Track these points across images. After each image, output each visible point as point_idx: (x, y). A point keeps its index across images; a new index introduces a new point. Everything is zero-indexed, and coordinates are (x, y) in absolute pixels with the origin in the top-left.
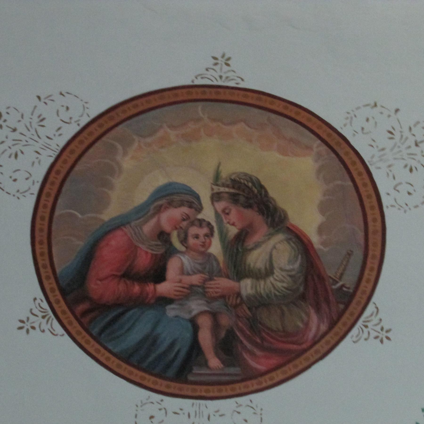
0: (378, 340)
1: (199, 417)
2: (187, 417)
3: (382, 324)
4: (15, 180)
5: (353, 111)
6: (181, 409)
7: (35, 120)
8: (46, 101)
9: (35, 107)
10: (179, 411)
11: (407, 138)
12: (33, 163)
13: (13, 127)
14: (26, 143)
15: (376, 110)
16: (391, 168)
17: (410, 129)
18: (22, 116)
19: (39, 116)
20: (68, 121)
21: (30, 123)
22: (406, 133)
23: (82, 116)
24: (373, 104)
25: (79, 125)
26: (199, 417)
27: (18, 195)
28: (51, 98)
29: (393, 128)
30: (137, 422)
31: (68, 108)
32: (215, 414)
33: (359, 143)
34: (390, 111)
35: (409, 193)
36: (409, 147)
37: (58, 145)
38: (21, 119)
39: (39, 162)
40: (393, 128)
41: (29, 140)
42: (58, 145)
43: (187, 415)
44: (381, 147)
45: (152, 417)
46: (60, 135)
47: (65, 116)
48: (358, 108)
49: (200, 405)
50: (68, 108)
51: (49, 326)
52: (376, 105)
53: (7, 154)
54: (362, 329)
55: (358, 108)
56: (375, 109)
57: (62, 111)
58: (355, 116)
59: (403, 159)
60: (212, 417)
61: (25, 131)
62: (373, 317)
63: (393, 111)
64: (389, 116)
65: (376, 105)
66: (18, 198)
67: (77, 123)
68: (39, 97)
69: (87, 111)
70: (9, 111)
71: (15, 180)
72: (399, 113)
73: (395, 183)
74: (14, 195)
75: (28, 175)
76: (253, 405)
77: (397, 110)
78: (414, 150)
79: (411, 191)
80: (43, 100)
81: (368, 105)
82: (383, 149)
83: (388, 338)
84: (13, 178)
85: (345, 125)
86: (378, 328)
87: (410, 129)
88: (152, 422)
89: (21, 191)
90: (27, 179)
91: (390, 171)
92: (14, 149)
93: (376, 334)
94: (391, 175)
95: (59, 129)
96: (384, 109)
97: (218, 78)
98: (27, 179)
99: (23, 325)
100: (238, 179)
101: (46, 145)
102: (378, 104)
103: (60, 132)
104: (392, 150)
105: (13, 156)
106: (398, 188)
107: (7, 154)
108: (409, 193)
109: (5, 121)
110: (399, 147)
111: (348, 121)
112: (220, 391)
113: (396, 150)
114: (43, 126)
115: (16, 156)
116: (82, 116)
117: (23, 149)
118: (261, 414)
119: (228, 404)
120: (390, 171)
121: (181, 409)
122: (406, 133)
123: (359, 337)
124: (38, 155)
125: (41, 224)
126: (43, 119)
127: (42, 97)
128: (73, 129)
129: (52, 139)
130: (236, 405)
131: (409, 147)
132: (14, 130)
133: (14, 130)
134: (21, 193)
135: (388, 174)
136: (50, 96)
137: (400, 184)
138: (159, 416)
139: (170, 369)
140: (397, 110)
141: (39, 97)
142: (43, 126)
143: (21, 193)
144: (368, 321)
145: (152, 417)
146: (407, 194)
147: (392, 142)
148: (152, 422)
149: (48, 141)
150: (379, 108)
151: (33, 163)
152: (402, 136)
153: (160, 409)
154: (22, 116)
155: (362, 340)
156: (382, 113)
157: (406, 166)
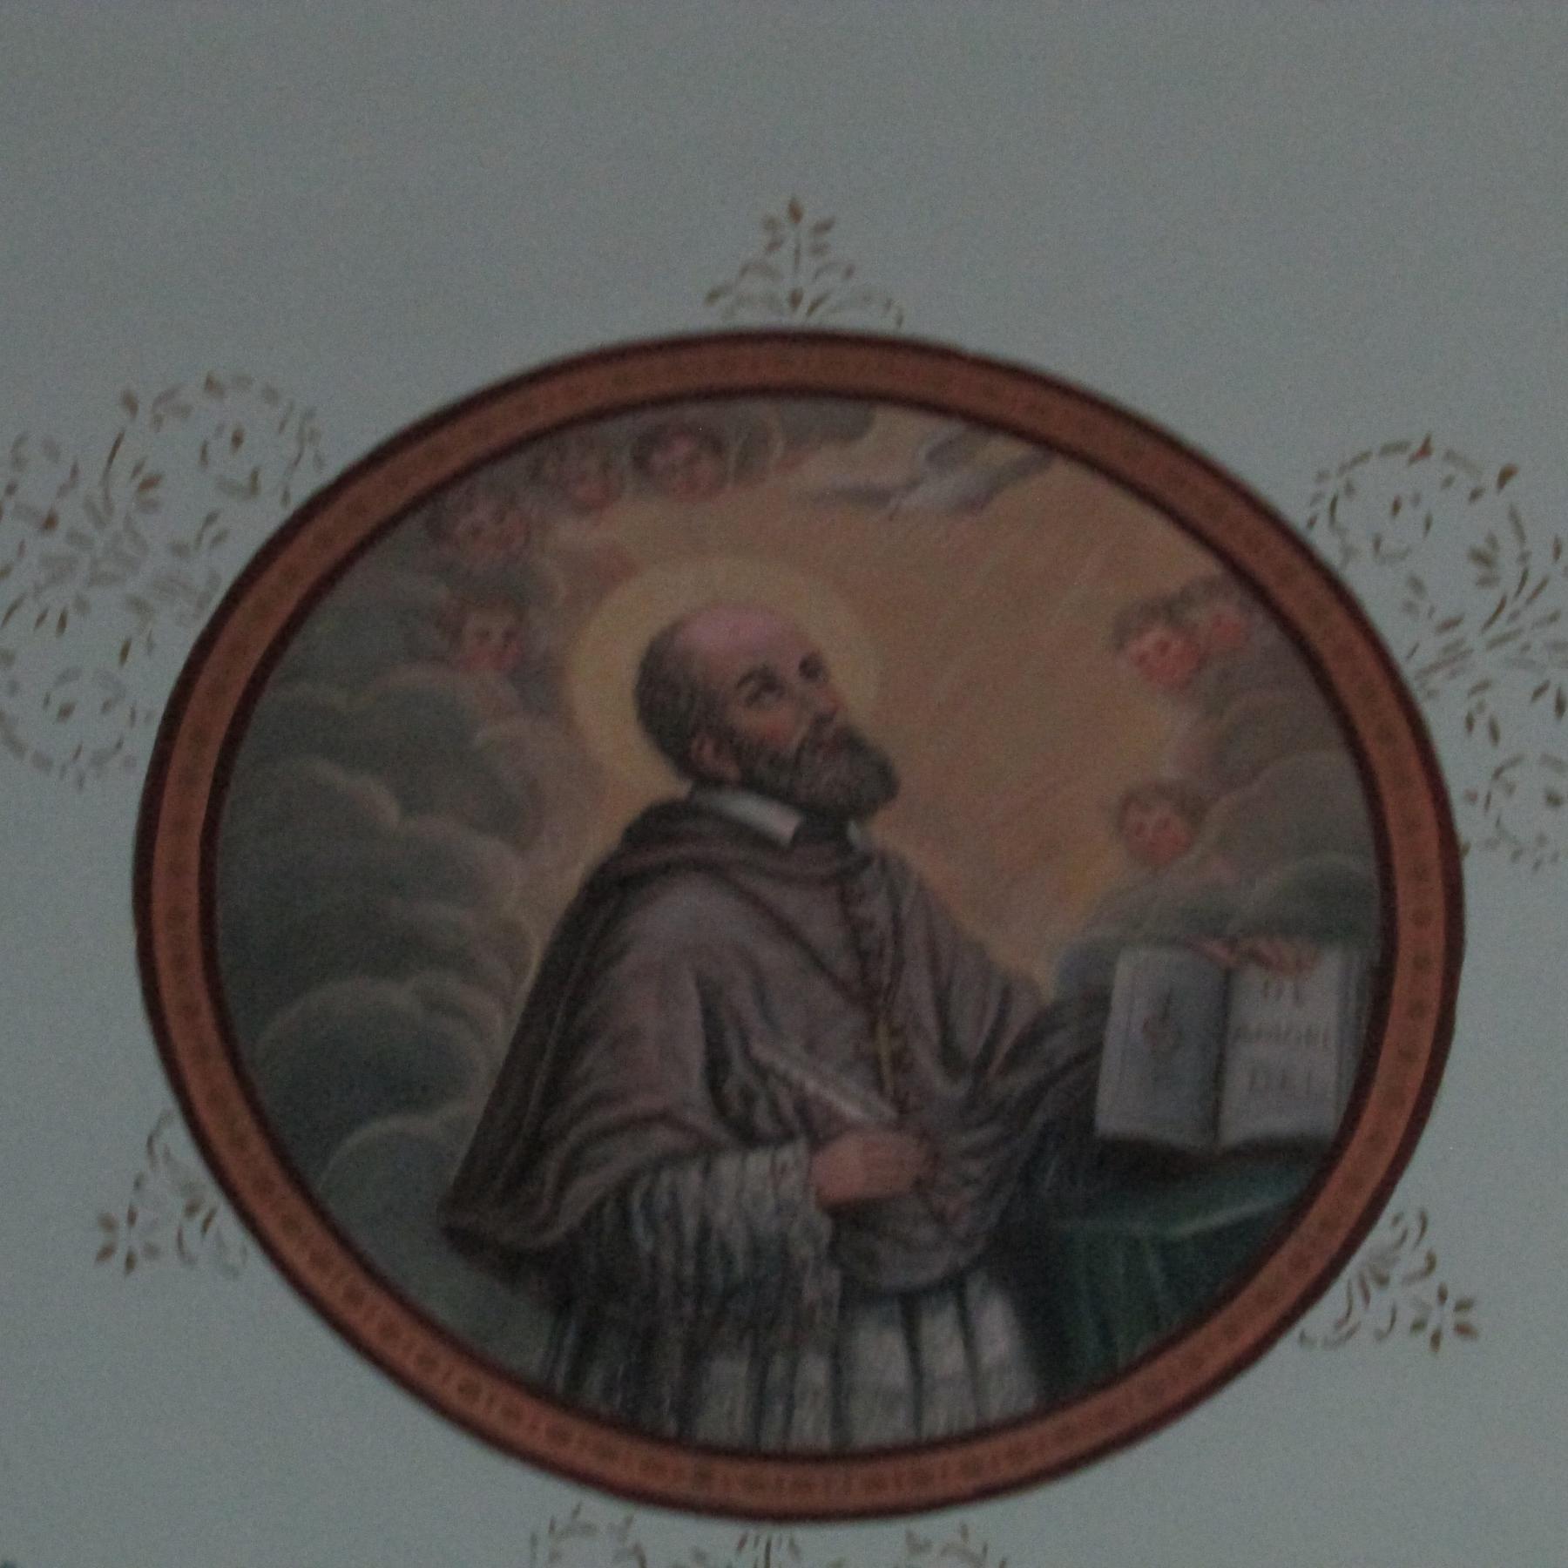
7: (124, 490)
15: (1433, 468)
19: (137, 469)
24: (1416, 447)
37: (742, 1544)
42: (742, 1544)
46: (1470, 723)
53: (29, 613)
54: (1363, 1285)
63: (1491, 479)
64: (1475, 495)
65: (1425, 451)
72: (1513, 485)
73: (1500, 756)
77: (1506, 476)
78: (71, 514)
81: (1399, 447)
82: (1450, 624)
83: (1436, 1339)
90: (1377, 544)
95: (211, 519)
99: (117, 1245)
102: (1435, 444)
106: (1510, 775)
112: (318, 1261)
123: (1345, 1329)
124: (1439, 617)
128: (266, 518)
137: (1515, 762)
139: (1395, 925)
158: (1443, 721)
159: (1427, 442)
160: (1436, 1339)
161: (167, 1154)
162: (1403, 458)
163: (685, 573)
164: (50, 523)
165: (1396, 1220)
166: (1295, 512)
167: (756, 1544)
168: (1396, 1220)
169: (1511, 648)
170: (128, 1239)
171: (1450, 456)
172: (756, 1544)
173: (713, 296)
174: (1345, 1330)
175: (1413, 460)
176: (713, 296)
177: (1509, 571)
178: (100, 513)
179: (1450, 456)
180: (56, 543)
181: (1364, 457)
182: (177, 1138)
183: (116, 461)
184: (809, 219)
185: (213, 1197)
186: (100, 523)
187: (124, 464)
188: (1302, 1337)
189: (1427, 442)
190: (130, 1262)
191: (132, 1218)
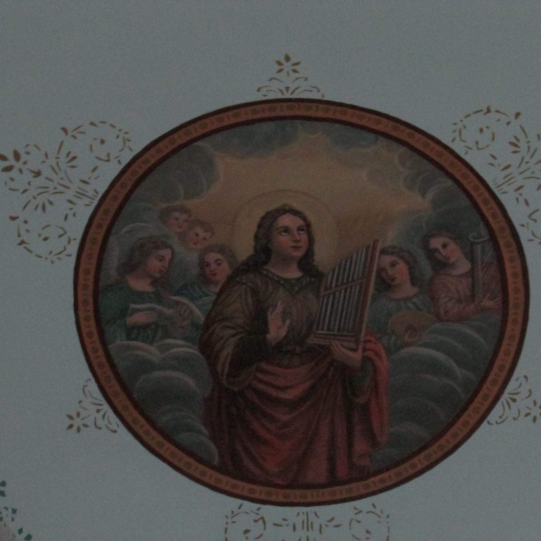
2: (292, 529)
3: (533, 397)
4: (46, 239)
5: (461, 121)
6: (285, 520)
7: (63, 159)
8: (75, 133)
9: (62, 143)
13: (36, 171)
14: (55, 191)
15: (493, 115)
18: (46, 155)
21: (58, 163)
24: (485, 110)
25: (119, 162)
26: (308, 530)
28: (79, 130)
29: (37, 207)
30: (229, 539)
31: (102, 142)
32: (328, 523)
33: (478, 161)
38: (45, 159)
39: (74, 215)
41: (58, 186)
43: (291, 527)
45: (247, 531)
49: (307, 513)
51: (106, 422)
52: (489, 111)
53: (521, 136)
54: (508, 403)
58: (465, 127)
61: (53, 176)
64: (508, 124)
67: (118, 159)
68: (65, 130)
69: (128, 144)
70: (28, 149)
71: (46, 239)
75: (62, 232)
76: (378, 511)
77: (518, 115)
78: (46, 172)
80: (70, 133)
84: (43, 236)
85: (454, 140)
88: (247, 538)
90: (60, 236)
92: (41, 199)
95: (95, 169)
96: (500, 114)
97: (284, 91)
98: (60, 236)
105: (40, 208)
107: (521, 136)
109: (25, 163)
111: (457, 134)
113: (524, 167)
115: (44, 208)
117: (52, 198)
120: (521, 195)
121: (285, 520)
125: (492, 208)
126: (74, 158)
127: (70, 129)
132: (38, 174)
133: (38, 174)
135: (517, 199)
138: (256, 529)
140: (518, 115)
141: (65, 130)
144: (517, 394)
145: (247, 531)
147: (518, 156)
148: (247, 538)
149: (83, 185)
150: (493, 114)
152: (529, 148)
153: (256, 521)
154: (46, 155)
158: (508, 201)
161: (311, 91)
162: (482, 113)
163: (244, 186)
165: (265, 96)
168: (265, 96)
169: (528, 174)
170: (77, 422)
174: (502, 420)
175: (486, 114)
180: (40, 181)
182: (493, 416)
183: (61, 151)
187: (64, 152)
188: (488, 422)
190: (79, 430)
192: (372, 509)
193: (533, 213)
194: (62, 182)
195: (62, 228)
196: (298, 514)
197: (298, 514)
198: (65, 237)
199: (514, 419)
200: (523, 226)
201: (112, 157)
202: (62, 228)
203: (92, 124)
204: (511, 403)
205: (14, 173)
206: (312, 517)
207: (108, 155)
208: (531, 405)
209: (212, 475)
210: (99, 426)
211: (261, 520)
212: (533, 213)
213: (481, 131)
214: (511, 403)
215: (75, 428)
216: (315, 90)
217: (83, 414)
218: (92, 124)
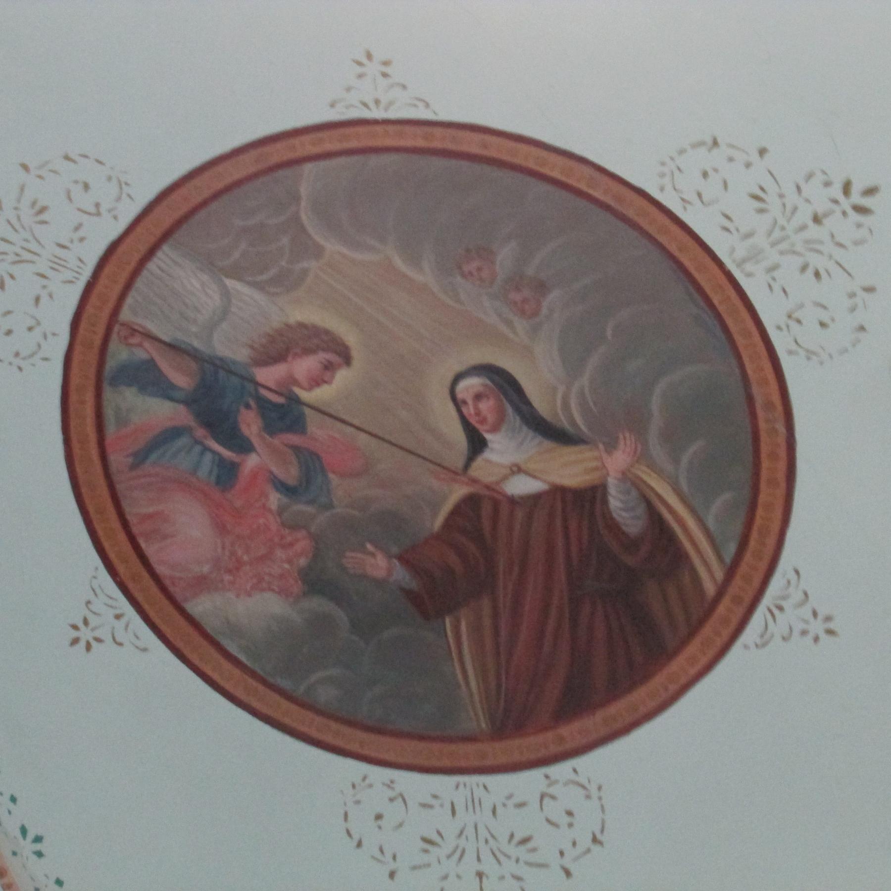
0: (809, 639)
1: (51, 261)
5: (672, 159)
7: (816, 261)
10: (430, 801)
11: (795, 209)
12: (37, 299)
14: (17, 258)
15: (585, 841)
16: (776, 274)
17: (799, 188)
19: (34, 204)
20: (92, 210)
22: (792, 198)
23: (119, 199)
24: (709, 141)
26: (51, 261)
27: (17, 361)
29: (762, 189)
34: (747, 153)
35: (823, 325)
36: (803, 228)
40: (762, 189)
44: (743, 230)
46: (435, 797)
47: (86, 201)
48: (682, 152)
50: (86, 187)
52: (715, 143)
53: (769, 184)
55: (682, 152)
56: (715, 151)
57: (77, 190)
59: (794, 252)
60: (499, 811)
62: (791, 590)
63: (567, 862)
64: (748, 165)
66: (20, 369)
68: (25, 167)
72: (767, 156)
74: (10, 364)
75: (32, 322)
77: (762, 152)
78: (814, 231)
79: (826, 320)
81: (701, 144)
83: (75, 627)
86: (806, 612)
87: (799, 188)
89: (23, 354)
91: (774, 279)
93: (801, 626)
94: (776, 287)
97: (372, 105)
100: (356, 513)
101: (56, 260)
103: (81, 233)
104: (770, 233)
107: (769, 184)
108: (823, 325)
110: (783, 228)
114: (44, 222)
116: (119, 199)
118: (600, 798)
119: (528, 782)
122: (792, 198)
124: (44, 282)
127: (32, 166)
129: (452, 804)
130: (546, 782)
131: (803, 228)
134: (24, 359)
136: (47, 163)
142: (44, 222)
143: (24, 359)
146: (818, 326)
149: (460, 809)
151: (37, 299)
155: (777, 639)
156: (731, 159)
157: (804, 268)
159: (601, 843)
160: (75, 627)
161: (415, 106)
164: (817, 220)
166: (582, 762)
167: (78, 267)
169: (784, 246)
171: (588, 851)
172: (78, 267)
173: (332, 105)
176: (332, 105)
177: (512, 850)
178: (812, 245)
179: (588, 851)
181: (603, 809)
184: (74, 634)
185: (767, 600)
186: (807, 242)
189: (601, 843)
190: (88, 647)
191: (385, 75)
192: (573, 776)
193: (89, 214)
194: (25, 245)
195: (33, 317)
196: (457, 787)
197: (457, 787)
198: (37, 331)
199: (784, 639)
200: (115, 218)
201: (103, 209)
202: (33, 317)
203: (67, 158)
204: (776, 612)
205: (836, 191)
206: (479, 792)
207: (97, 205)
208: (809, 616)
209: (498, 751)
210: (118, 639)
211: (400, 799)
212: (89, 214)
213: (705, 175)
214: (776, 612)
215: (82, 644)
216: (421, 105)
217: (93, 621)
218: (67, 158)
